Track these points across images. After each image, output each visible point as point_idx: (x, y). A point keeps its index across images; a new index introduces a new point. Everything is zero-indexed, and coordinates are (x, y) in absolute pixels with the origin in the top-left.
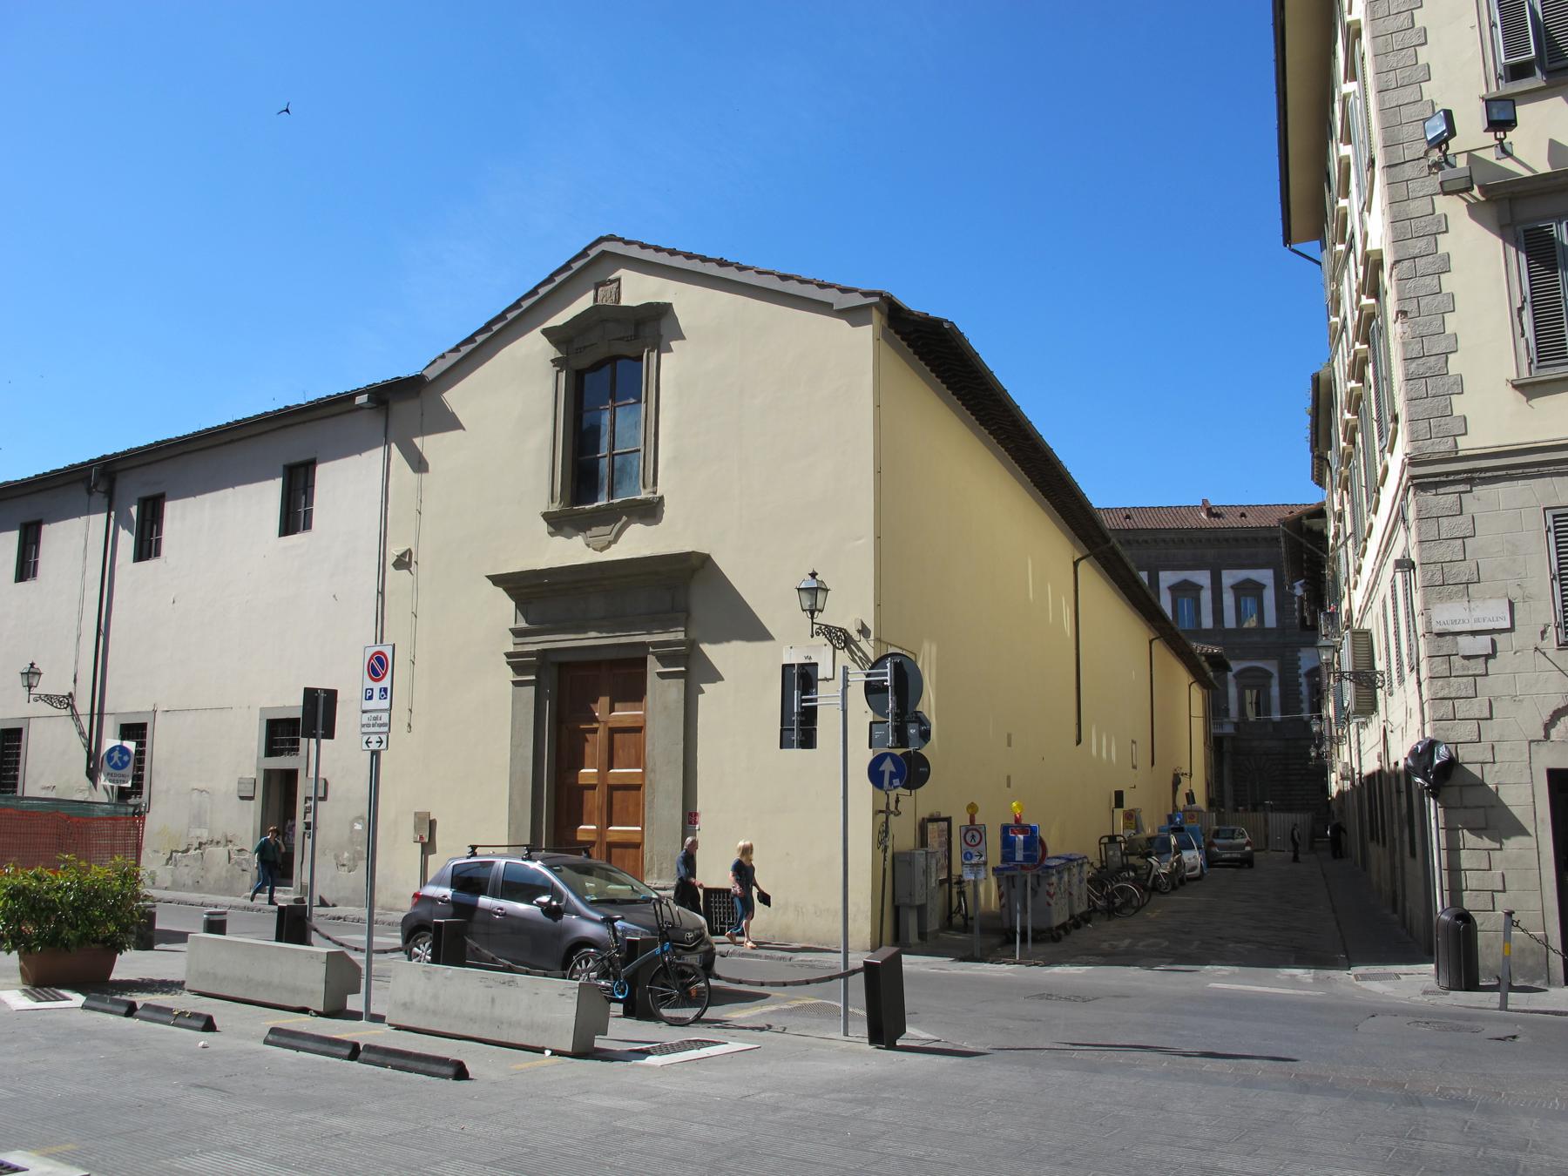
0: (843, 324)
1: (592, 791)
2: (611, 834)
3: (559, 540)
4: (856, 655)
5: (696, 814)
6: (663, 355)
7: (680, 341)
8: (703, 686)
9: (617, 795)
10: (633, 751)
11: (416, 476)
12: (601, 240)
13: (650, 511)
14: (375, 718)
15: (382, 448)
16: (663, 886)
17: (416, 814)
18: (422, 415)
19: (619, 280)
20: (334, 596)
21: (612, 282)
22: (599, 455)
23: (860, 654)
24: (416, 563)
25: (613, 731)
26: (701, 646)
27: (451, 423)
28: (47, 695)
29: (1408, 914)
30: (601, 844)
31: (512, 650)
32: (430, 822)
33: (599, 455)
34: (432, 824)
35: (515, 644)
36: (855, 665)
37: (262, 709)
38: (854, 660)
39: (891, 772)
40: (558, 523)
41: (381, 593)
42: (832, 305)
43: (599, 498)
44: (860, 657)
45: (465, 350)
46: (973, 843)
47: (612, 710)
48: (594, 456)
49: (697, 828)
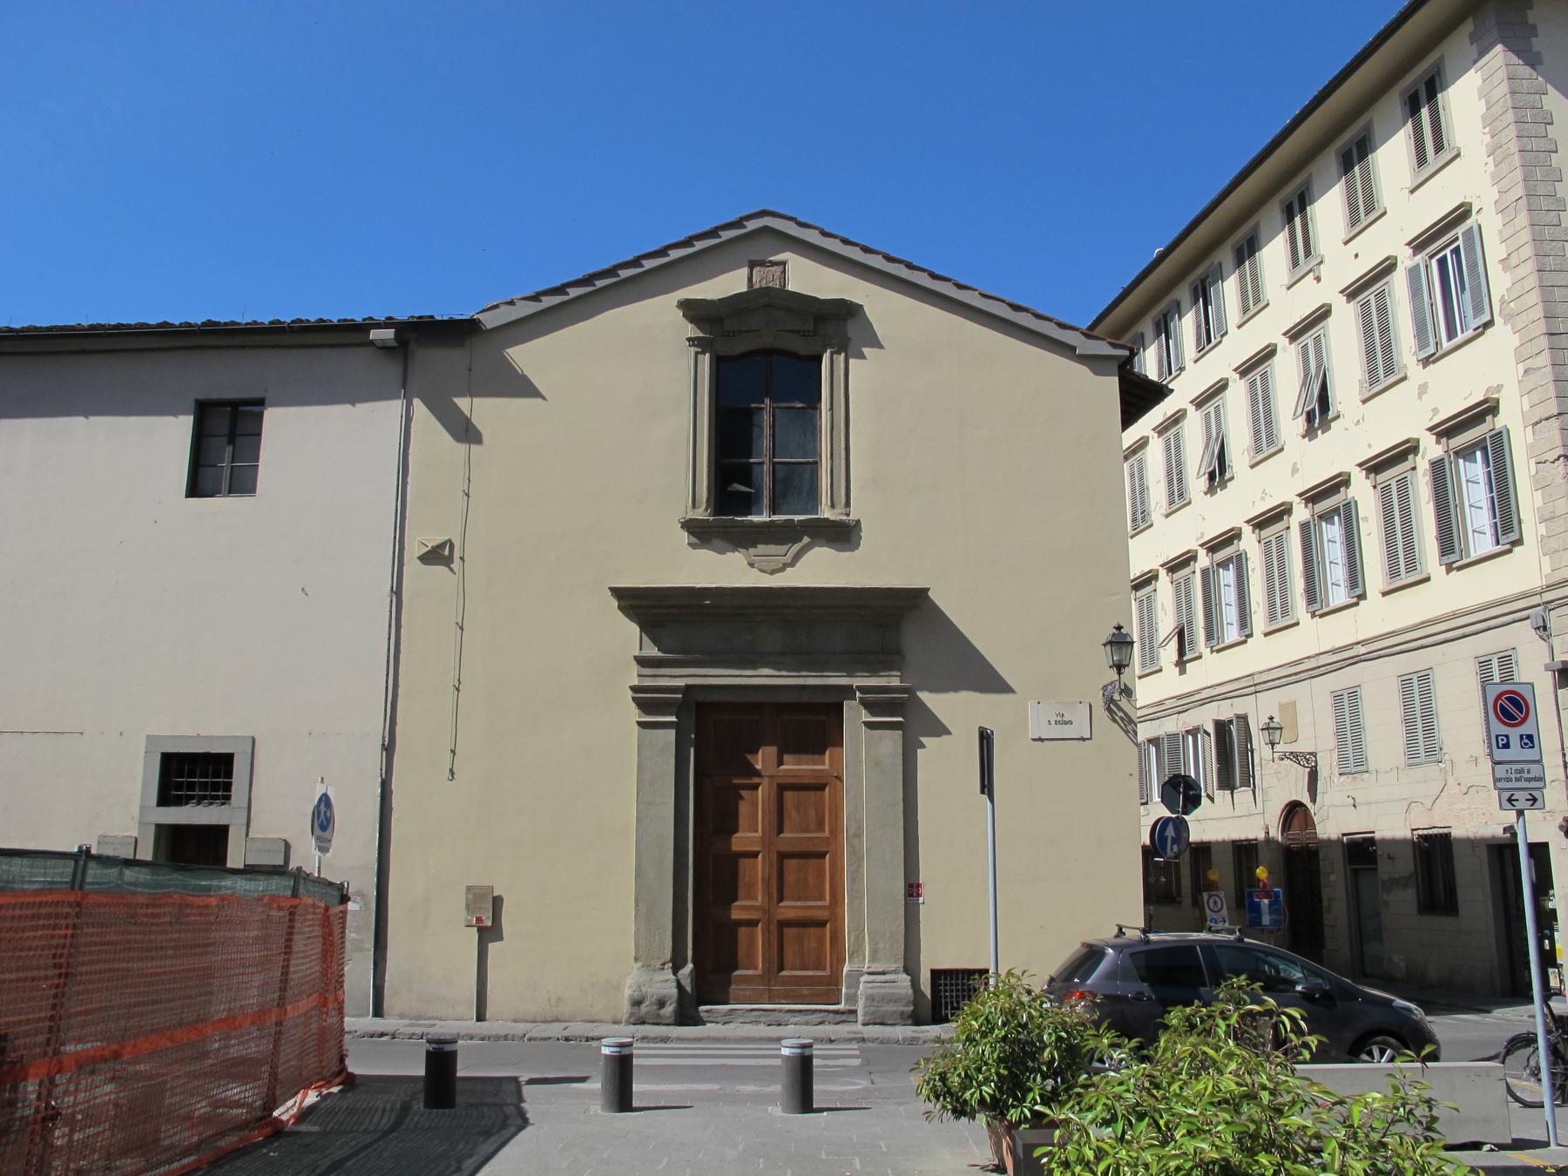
0: (1083, 371)
1: (752, 860)
2: (783, 910)
3: (705, 555)
4: (1116, 714)
5: (919, 886)
6: (851, 361)
7: (877, 350)
8: (923, 739)
9: (790, 865)
10: (812, 812)
11: (463, 447)
12: (763, 213)
13: (843, 535)
14: (1522, 771)
15: (400, 402)
16: (881, 970)
17: (469, 889)
18: (470, 370)
19: (784, 263)
20: (303, 589)
21: (773, 264)
22: (752, 460)
23: (1121, 714)
24: (462, 559)
25: (782, 788)
26: (918, 693)
27: (523, 388)
28: (1292, 753)
29: (1292, 965)
30: (769, 922)
31: (636, 683)
32: (495, 899)
33: (752, 460)
34: (497, 902)
35: (639, 676)
36: (1116, 725)
37: (150, 739)
38: (1114, 720)
39: (1172, 837)
40: (700, 533)
41: (397, 592)
42: (1074, 349)
43: (753, 509)
44: (1121, 718)
45: (548, 301)
46: (1216, 909)
47: (780, 763)
48: (744, 461)
49: (921, 901)
